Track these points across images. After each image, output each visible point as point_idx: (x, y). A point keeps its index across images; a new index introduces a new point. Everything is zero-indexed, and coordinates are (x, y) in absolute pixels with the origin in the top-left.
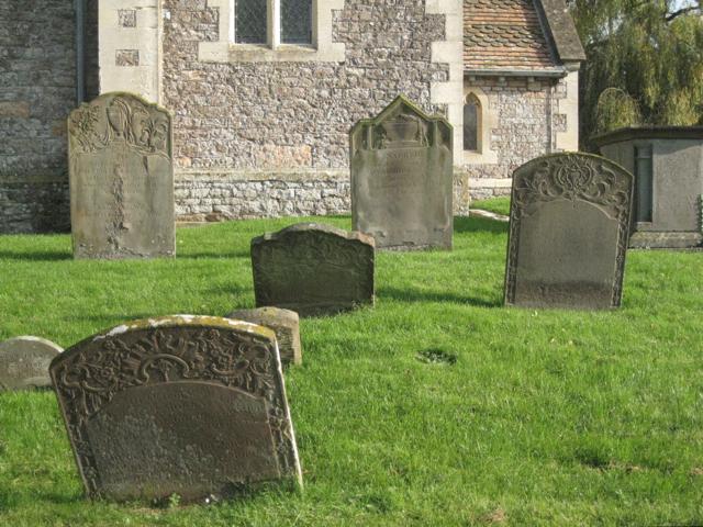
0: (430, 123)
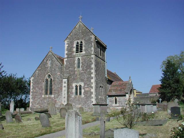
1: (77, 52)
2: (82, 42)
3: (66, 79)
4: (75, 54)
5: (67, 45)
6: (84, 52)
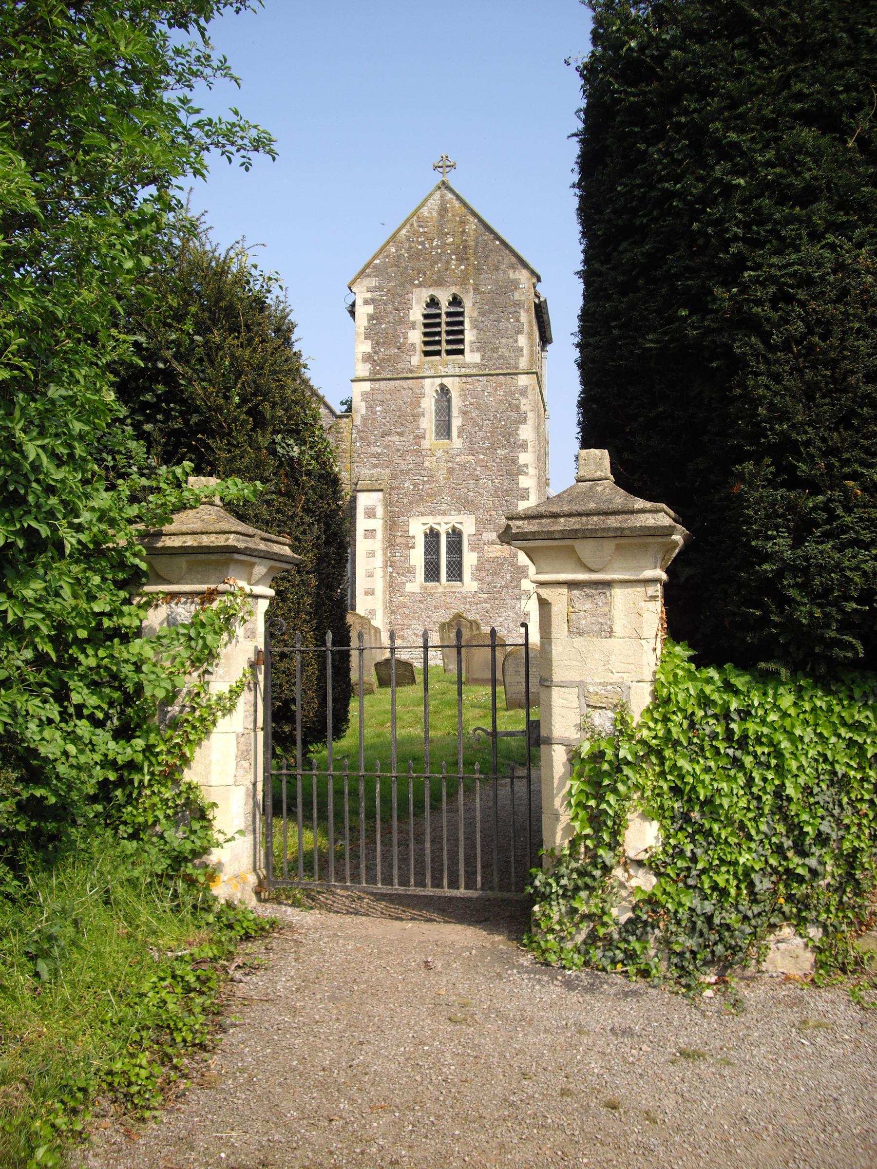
0: (470, 622)
1: (427, 354)
2: (456, 301)
3: (380, 494)
4: (416, 359)
5: (370, 309)
6: (472, 357)
